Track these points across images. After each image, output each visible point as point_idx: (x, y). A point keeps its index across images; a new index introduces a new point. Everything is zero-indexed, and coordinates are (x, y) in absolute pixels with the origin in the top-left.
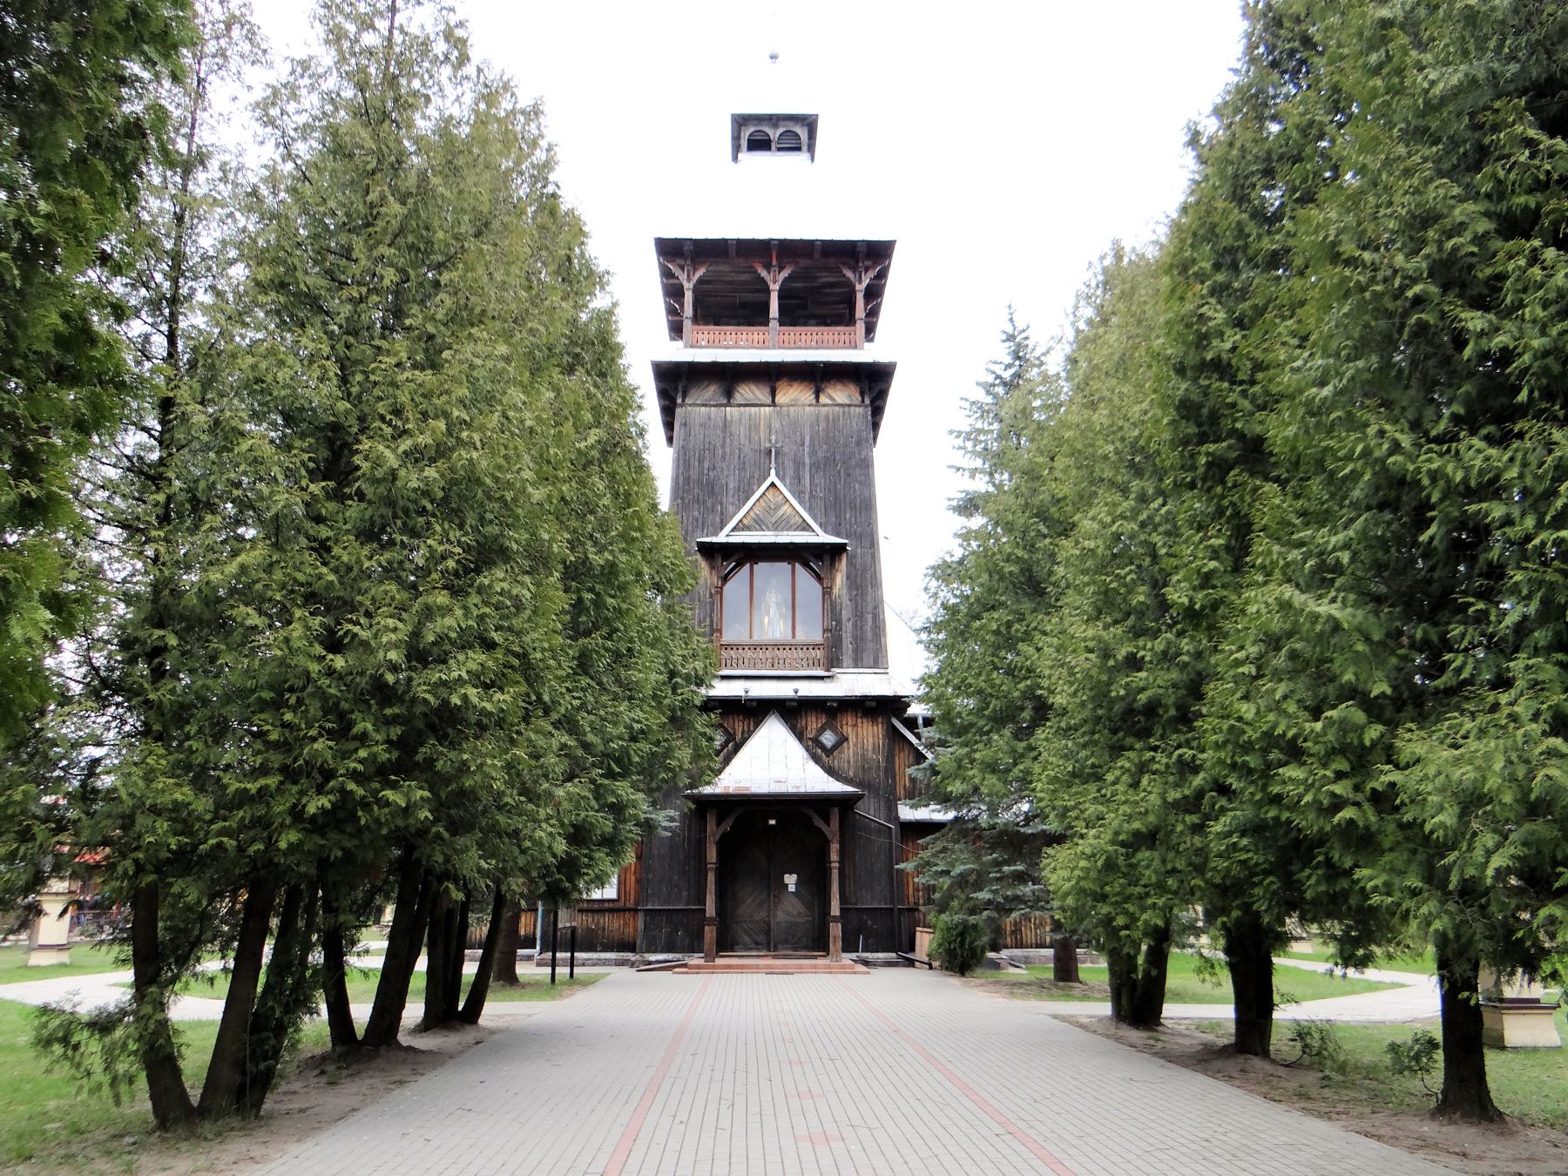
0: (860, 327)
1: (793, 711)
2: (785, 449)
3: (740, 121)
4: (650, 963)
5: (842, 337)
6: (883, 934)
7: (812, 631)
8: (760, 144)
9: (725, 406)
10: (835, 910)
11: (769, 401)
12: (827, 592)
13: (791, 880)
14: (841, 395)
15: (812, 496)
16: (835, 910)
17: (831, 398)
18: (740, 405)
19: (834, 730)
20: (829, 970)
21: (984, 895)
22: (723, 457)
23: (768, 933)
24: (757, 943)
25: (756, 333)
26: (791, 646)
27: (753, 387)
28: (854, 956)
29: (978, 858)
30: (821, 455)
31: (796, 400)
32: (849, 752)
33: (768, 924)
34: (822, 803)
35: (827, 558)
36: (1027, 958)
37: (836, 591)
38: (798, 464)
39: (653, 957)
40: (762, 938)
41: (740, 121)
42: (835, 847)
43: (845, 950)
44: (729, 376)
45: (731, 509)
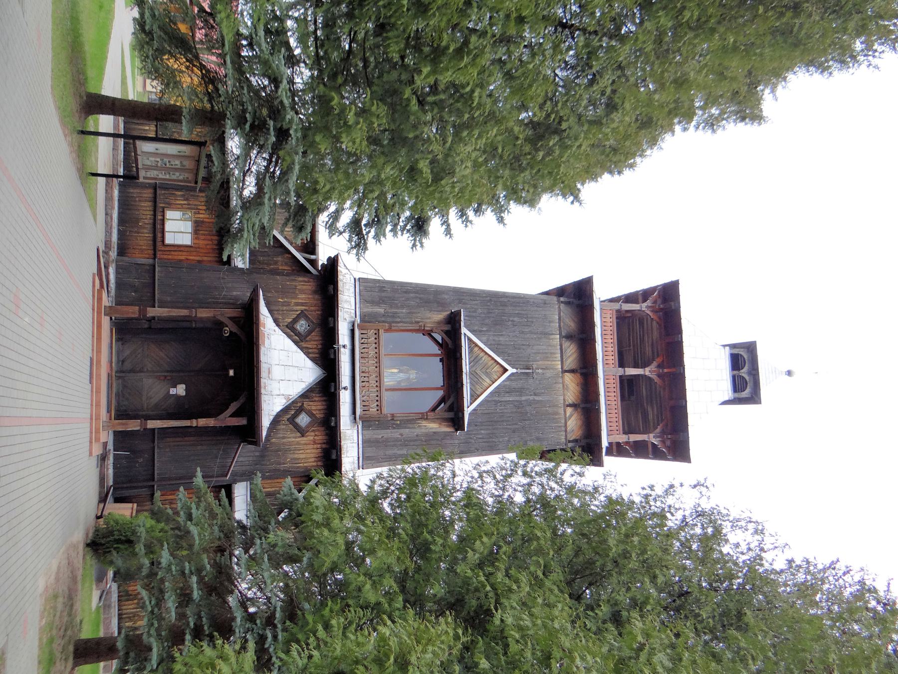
0: (622, 438)
1: (327, 387)
2: (531, 381)
3: (751, 348)
4: (106, 267)
5: (615, 424)
6: (132, 470)
7: (391, 404)
8: (736, 362)
9: (560, 334)
10: (152, 424)
11: (566, 368)
12: (424, 417)
13: (180, 390)
14: (573, 424)
15: (497, 402)
16: (152, 424)
17: (571, 416)
18: (561, 346)
19: (310, 425)
20: (94, 418)
21: (165, 557)
22: (523, 332)
23: (132, 371)
24: (123, 361)
25: (613, 358)
26: (379, 387)
27: (575, 356)
28: (110, 446)
29: (205, 550)
30: (528, 409)
31: (567, 389)
32: (292, 438)
33: (141, 371)
34: (251, 408)
35: (451, 415)
36: (109, 606)
37: (424, 423)
38: (520, 391)
39: (112, 270)
40: (128, 365)
41: (751, 348)
42: (210, 422)
43: (116, 434)
44: (583, 338)
45: (484, 338)
